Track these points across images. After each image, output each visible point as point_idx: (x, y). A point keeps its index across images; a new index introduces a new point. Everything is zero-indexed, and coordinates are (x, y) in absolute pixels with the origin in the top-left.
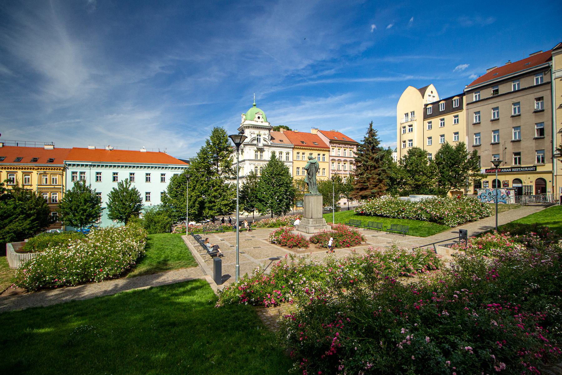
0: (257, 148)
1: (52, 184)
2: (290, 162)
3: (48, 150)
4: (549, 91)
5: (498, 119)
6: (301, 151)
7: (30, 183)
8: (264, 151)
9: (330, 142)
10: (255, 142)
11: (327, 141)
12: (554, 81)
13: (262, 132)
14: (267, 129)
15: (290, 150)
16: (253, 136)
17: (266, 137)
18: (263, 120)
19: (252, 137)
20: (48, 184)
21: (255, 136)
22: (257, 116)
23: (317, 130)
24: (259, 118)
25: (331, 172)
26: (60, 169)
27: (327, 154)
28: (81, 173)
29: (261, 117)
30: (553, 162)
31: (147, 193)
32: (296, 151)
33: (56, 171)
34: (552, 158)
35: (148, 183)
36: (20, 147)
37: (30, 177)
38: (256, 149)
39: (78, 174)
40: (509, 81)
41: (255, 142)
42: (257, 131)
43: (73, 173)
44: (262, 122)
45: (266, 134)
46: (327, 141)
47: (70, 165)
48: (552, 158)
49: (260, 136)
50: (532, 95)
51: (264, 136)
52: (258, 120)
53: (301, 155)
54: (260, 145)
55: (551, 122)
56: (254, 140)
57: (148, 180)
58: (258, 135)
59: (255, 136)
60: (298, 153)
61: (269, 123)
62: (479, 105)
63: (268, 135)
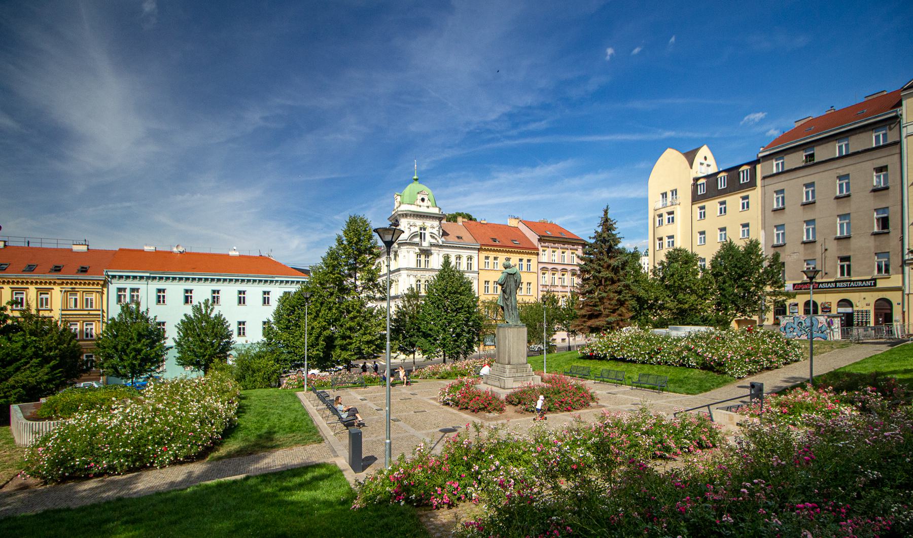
0: (420, 249)
1: (85, 308)
2: (474, 272)
3: (78, 253)
4: (897, 157)
5: (814, 203)
6: (492, 255)
7: (49, 307)
8: (431, 254)
9: (540, 240)
10: (417, 240)
11: (533, 238)
12: (904, 141)
13: (428, 223)
14: (437, 217)
15: (474, 253)
16: (414, 229)
17: (435, 231)
18: (429, 204)
19: (412, 232)
20: (78, 307)
21: (417, 229)
22: (420, 197)
23: (517, 221)
24: (423, 200)
25: (541, 288)
26: (98, 284)
27: (534, 258)
28: (133, 290)
29: (426, 199)
30: (903, 273)
31: (240, 323)
32: (483, 254)
33: (91, 287)
34: (902, 266)
35: (242, 307)
36: (32, 248)
37: (48, 296)
38: (418, 251)
39: (128, 291)
40: (830, 139)
41: (417, 240)
42: (419, 222)
43: (120, 290)
44: (428, 207)
45: (435, 226)
46: (533, 238)
47: (114, 277)
48: (902, 266)
49: (425, 229)
50: (869, 163)
51: (431, 230)
52: (421, 203)
53: (491, 260)
54: (425, 244)
55: (900, 207)
56: (415, 236)
57: (241, 301)
58: (421, 229)
59: (417, 229)
60: (487, 258)
61: (440, 209)
62: (783, 179)
63: (437, 228)
